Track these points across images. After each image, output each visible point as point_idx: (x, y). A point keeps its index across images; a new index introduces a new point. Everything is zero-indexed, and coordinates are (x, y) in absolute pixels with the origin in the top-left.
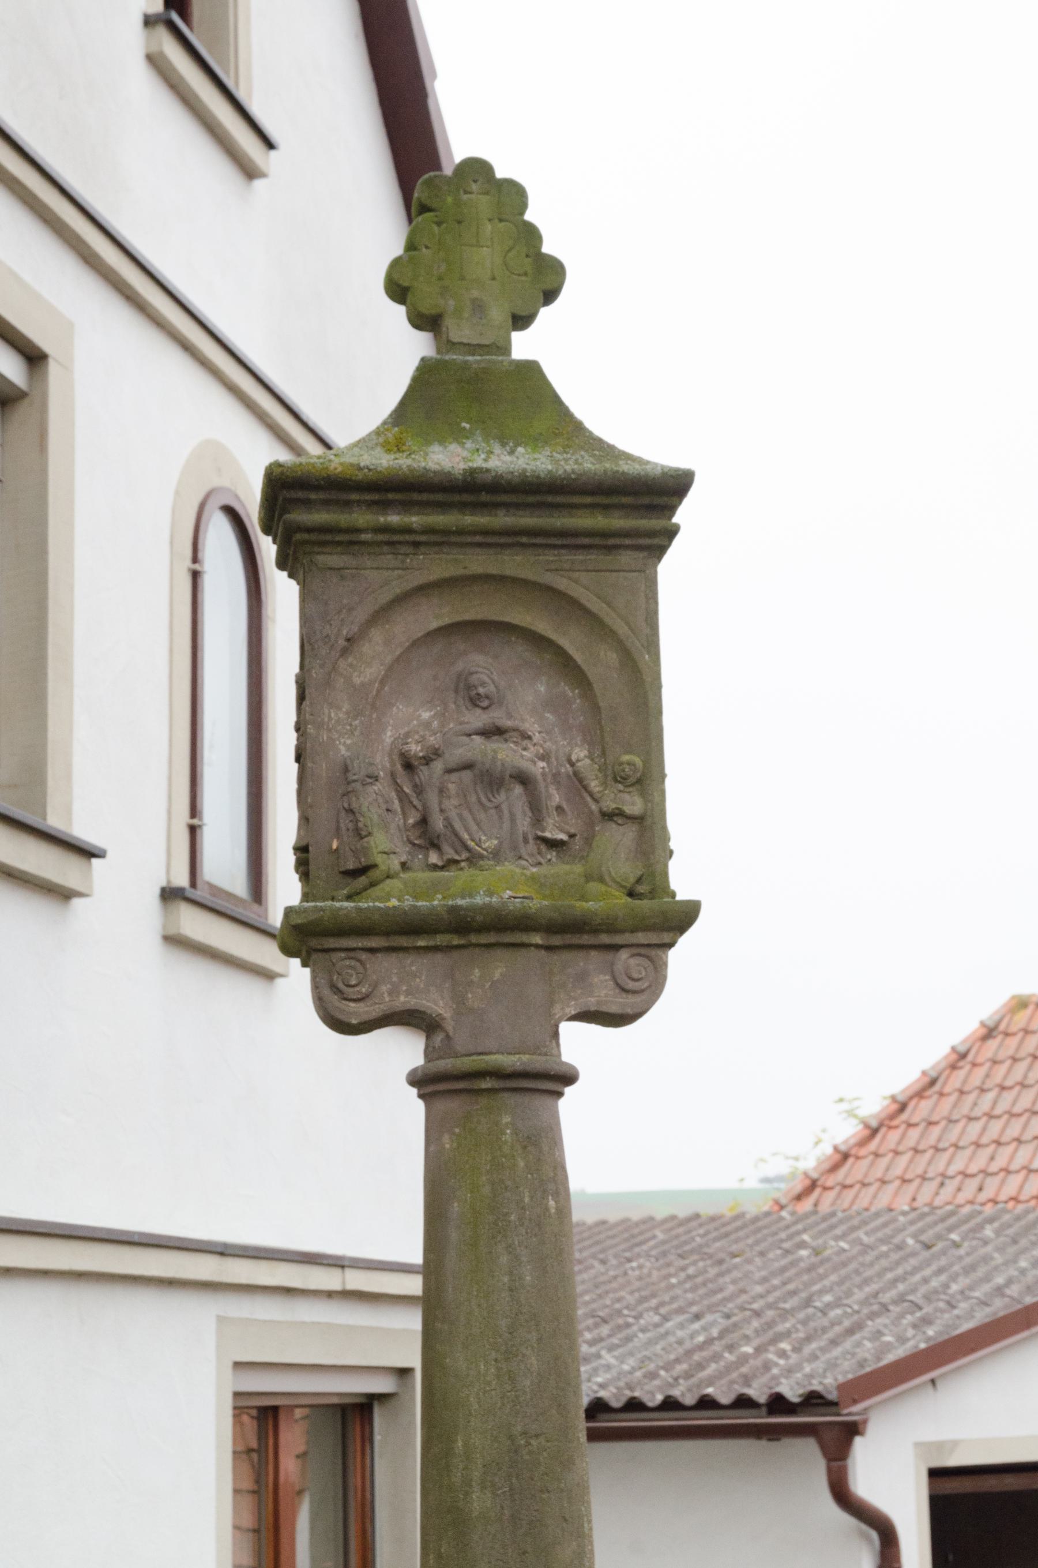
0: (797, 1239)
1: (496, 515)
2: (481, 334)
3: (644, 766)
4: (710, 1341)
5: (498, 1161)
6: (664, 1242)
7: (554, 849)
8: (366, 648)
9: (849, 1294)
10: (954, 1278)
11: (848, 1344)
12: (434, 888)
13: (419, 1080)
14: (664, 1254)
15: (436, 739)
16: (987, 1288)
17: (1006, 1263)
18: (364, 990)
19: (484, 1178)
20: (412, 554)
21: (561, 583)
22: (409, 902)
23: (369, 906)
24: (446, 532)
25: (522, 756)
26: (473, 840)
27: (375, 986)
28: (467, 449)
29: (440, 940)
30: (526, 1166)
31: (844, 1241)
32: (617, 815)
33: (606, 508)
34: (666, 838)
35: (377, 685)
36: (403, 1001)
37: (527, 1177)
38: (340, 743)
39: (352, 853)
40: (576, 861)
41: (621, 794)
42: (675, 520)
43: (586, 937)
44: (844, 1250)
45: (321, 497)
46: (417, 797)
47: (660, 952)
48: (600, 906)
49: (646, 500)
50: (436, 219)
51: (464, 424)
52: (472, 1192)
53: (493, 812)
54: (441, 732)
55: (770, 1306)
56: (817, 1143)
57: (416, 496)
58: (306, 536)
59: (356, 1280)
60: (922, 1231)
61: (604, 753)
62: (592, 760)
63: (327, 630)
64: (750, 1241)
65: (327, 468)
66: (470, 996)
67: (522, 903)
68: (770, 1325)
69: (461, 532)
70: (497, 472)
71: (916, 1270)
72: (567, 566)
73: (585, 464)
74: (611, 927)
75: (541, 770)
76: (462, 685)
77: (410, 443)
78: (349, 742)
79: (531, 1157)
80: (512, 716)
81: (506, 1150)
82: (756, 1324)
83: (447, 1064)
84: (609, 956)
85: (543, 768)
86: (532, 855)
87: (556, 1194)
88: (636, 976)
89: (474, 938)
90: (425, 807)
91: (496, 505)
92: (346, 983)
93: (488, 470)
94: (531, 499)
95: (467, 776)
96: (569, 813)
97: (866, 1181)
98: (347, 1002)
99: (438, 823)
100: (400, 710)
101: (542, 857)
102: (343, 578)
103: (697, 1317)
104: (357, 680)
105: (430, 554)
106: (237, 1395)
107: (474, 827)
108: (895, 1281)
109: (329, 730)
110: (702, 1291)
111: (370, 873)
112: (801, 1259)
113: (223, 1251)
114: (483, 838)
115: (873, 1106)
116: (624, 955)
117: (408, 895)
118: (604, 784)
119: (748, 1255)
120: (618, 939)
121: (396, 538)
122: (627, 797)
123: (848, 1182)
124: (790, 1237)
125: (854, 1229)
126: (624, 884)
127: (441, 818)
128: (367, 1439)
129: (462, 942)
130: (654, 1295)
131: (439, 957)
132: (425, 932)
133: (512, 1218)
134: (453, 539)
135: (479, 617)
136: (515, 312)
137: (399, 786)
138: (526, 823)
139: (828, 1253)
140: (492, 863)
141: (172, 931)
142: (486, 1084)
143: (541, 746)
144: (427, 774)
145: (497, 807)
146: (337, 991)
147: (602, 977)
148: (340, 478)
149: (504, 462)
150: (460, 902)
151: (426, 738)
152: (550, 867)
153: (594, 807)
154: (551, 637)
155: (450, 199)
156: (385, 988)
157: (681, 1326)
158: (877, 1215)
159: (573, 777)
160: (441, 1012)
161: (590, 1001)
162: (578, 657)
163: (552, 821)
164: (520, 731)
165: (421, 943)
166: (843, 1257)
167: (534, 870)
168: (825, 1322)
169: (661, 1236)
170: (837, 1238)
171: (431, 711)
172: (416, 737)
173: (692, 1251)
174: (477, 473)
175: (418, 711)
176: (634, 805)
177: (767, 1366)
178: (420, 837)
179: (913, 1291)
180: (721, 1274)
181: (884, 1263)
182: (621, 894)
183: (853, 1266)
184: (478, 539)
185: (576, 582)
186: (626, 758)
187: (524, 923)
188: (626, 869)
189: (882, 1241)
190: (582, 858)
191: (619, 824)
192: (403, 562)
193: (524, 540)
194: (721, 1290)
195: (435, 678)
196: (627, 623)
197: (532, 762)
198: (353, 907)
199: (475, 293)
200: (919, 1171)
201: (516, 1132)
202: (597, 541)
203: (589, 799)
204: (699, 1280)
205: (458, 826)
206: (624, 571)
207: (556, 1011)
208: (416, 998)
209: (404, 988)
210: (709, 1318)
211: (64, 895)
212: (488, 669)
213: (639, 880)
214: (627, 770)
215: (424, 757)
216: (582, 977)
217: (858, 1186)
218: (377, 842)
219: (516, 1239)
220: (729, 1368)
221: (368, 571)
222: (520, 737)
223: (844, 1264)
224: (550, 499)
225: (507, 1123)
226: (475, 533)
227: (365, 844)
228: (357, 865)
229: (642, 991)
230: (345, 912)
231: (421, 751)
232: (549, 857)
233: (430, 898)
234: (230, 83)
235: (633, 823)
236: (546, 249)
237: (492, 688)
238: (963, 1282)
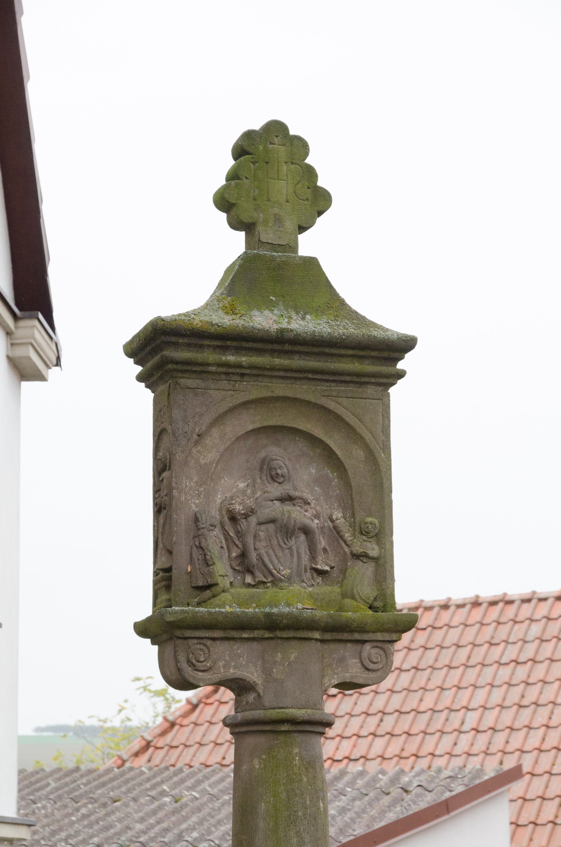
0: (159, 789)
1: (293, 359)
2: (280, 238)
3: (380, 526)
5: (291, 777)
6: (57, 789)
7: (320, 576)
8: (208, 441)
9: (210, 832)
14: (60, 797)
15: (250, 502)
18: (208, 665)
19: (282, 788)
20: (239, 381)
21: (331, 405)
23: (216, 611)
25: (305, 515)
26: (275, 569)
27: (215, 662)
28: (275, 314)
29: (257, 634)
30: (308, 780)
31: (194, 791)
32: (363, 556)
33: (360, 358)
35: (214, 465)
37: (308, 788)
38: (192, 502)
39: (201, 575)
40: (334, 584)
41: (365, 543)
42: (400, 365)
43: (346, 634)
44: (197, 799)
45: (186, 341)
46: (238, 539)
47: (389, 645)
48: (357, 616)
49: (385, 354)
50: (252, 160)
51: (271, 297)
52: (274, 797)
53: (287, 551)
54: (254, 497)
56: (120, 711)
57: (244, 344)
58: (175, 366)
61: (353, 515)
62: (345, 519)
63: (186, 428)
64: (123, 789)
65: (192, 323)
66: (275, 670)
67: (311, 612)
69: (272, 369)
70: (297, 332)
72: (334, 394)
74: (362, 629)
75: (316, 525)
76: (265, 467)
77: (241, 309)
78: (197, 502)
79: (310, 774)
80: (297, 489)
81: (296, 770)
83: (260, 714)
84: (358, 647)
85: (317, 524)
86: (309, 580)
88: (375, 660)
89: (279, 634)
90: (244, 545)
92: (198, 660)
93: (292, 330)
94: (316, 350)
95: (271, 527)
96: (330, 553)
97: (188, 744)
98: (197, 672)
99: (253, 557)
101: (314, 581)
102: (196, 395)
104: (202, 462)
105: (250, 382)
107: (276, 561)
109: (186, 494)
110: (96, 827)
111: (213, 589)
112: (165, 804)
114: (282, 568)
116: (367, 646)
117: (234, 603)
118: (354, 535)
119: (124, 800)
120: (365, 637)
121: (230, 370)
122: (368, 544)
123: (174, 744)
124: (153, 787)
125: (199, 782)
126: (368, 601)
127: (255, 554)
129: (271, 635)
130: (61, 829)
131: (255, 645)
132: (248, 629)
133: (300, 814)
134: (266, 373)
135: (279, 423)
136: (301, 224)
137: (226, 531)
138: (306, 559)
139: (184, 800)
140: (286, 584)
143: (315, 509)
144: (245, 525)
145: (290, 548)
146: (189, 662)
147: (354, 660)
148: (200, 330)
149: (301, 325)
150: (275, 610)
151: (245, 501)
152: (319, 588)
153: (347, 550)
154: (322, 439)
155: (261, 148)
156: (221, 664)
159: (333, 530)
160: (256, 680)
161: (347, 675)
163: (321, 558)
164: (303, 499)
165: (245, 635)
166: (197, 803)
167: (311, 589)
169: (53, 785)
171: (245, 483)
172: (238, 500)
173: (81, 796)
174: (285, 332)
175: (237, 482)
176: (373, 550)
178: (239, 565)
180: (108, 815)
182: (365, 607)
183: (206, 811)
184: (281, 373)
185: (340, 404)
186: (370, 519)
190: (338, 582)
191: (364, 562)
192: (234, 386)
193: (310, 376)
194: (111, 827)
195: (247, 461)
196: (371, 433)
197: (311, 519)
198: (206, 611)
199: (276, 210)
200: (212, 737)
201: (301, 759)
202: (355, 379)
203: (343, 544)
204: (93, 818)
205: (266, 559)
206: (369, 399)
207: (326, 681)
208: (240, 671)
209: (233, 664)
212: (283, 458)
213: (375, 599)
214: (370, 527)
215: (244, 514)
216: (342, 660)
217: (182, 747)
218: (218, 569)
219: (302, 827)
221: (212, 391)
222: (303, 503)
223: (199, 810)
224: (327, 350)
225: (296, 753)
226: (279, 370)
227: (211, 570)
228: (205, 583)
229: (378, 670)
230: (201, 614)
231: (243, 510)
232: (318, 581)
233: (248, 606)
235: (372, 561)
236: (320, 183)
237: (286, 470)
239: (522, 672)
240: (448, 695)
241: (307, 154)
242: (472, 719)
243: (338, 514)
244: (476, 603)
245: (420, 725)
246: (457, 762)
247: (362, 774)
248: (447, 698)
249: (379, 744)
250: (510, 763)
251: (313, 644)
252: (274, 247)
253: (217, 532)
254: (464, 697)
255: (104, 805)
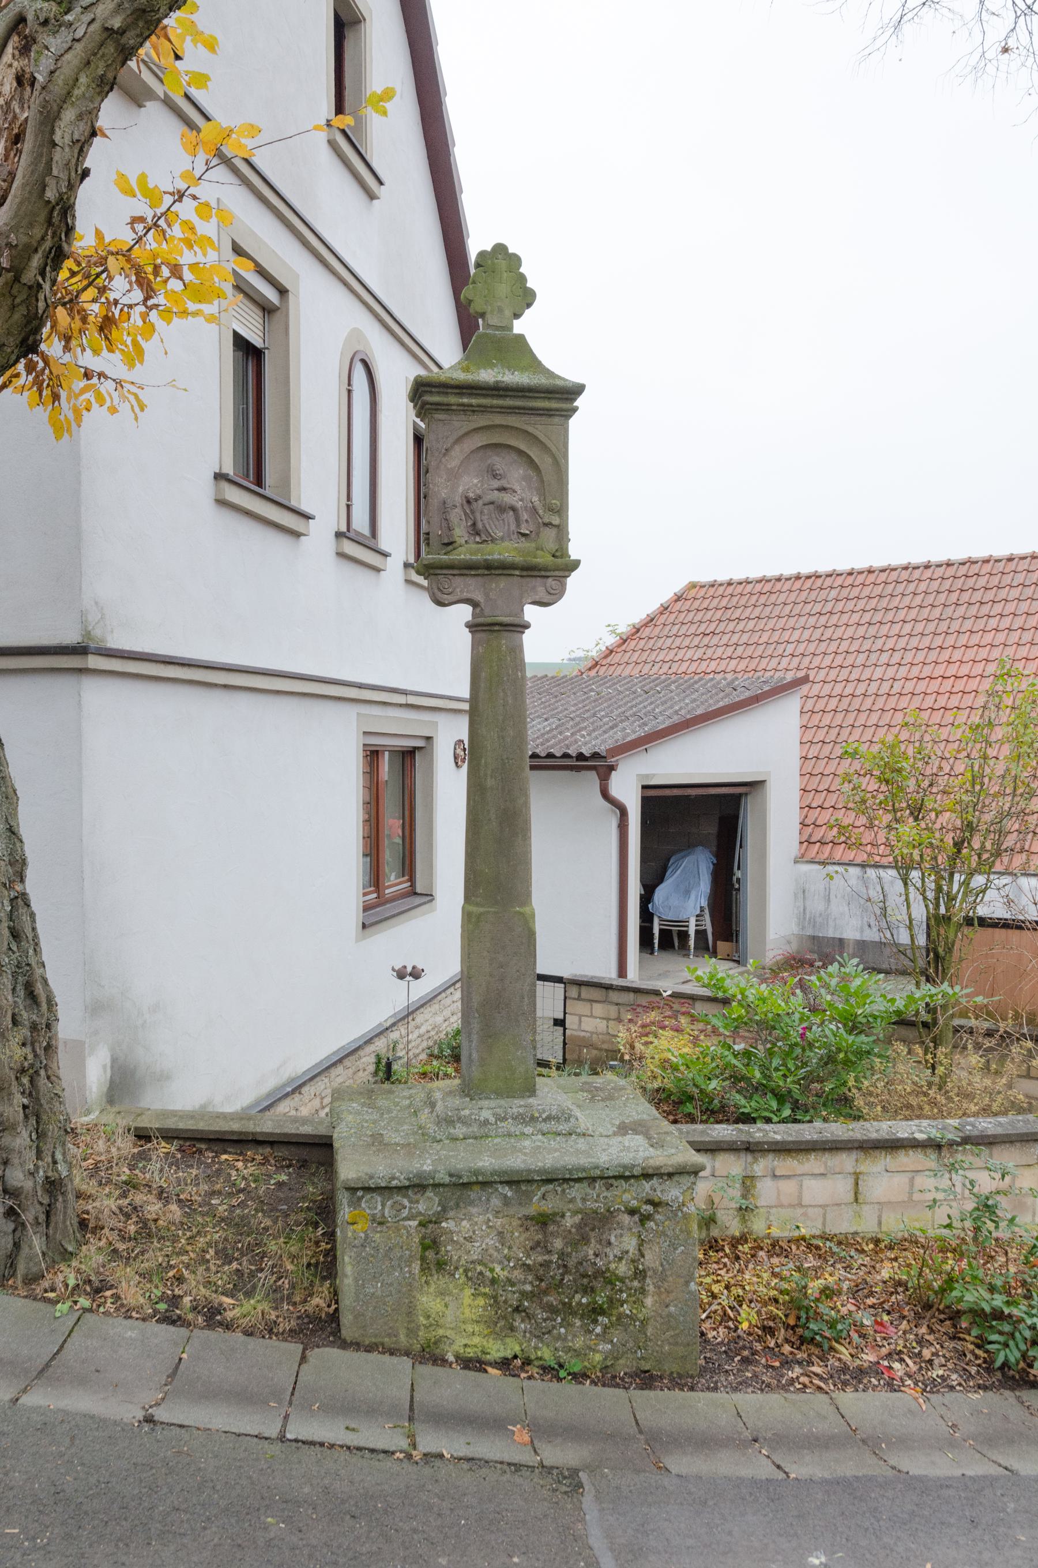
4: (551, 730)
8: (453, 453)
9: (612, 712)
10: (657, 706)
11: (611, 733)
12: (478, 551)
13: (470, 626)
16: (671, 711)
17: (680, 701)
21: (530, 429)
22: (468, 557)
24: (485, 407)
29: (480, 572)
34: (568, 533)
36: (465, 595)
42: (575, 404)
49: (565, 396)
55: (577, 716)
57: (474, 391)
59: (412, 700)
60: (644, 686)
68: (577, 724)
69: (491, 407)
71: (641, 703)
73: (541, 380)
74: (546, 569)
82: (571, 723)
87: (521, 671)
91: (506, 396)
94: (520, 394)
95: (491, 507)
99: (480, 525)
100: (466, 479)
103: (546, 720)
106: (364, 745)
108: (631, 707)
113: (361, 686)
115: (623, 629)
116: (550, 580)
120: (548, 574)
124: (586, 687)
128: (413, 765)
141: (340, 551)
142: (497, 628)
146: (439, 589)
150: (490, 557)
157: (539, 723)
158: (625, 678)
162: (536, 460)
168: (601, 723)
170: (607, 688)
176: (556, 520)
177: (576, 742)
179: (640, 711)
181: (627, 699)
187: (513, 566)
188: (552, 546)
189: (627, 690)
199: (499, 304)
205: (488, 526)
210: (551, 720)
211: (296, 535)
216: (534, 588)
220: (560, 742)
234: (363, 152)
236: (529, 285)
238: (661, 708)
239: (823, 620)
240: (777, 634)
241: (520, 265)
242: (790, 648)
243: (535, 499)
244: (798, 577)
245: (759, 652)
246: (768, 674)
247: (712, 679)
248: (776, 637)
249: (733, 663)
250: (801, 674)
251: (515, 578)
252: (497, 328)
253: (458, 510)
254: (786, 635)
255: (556, 697)
